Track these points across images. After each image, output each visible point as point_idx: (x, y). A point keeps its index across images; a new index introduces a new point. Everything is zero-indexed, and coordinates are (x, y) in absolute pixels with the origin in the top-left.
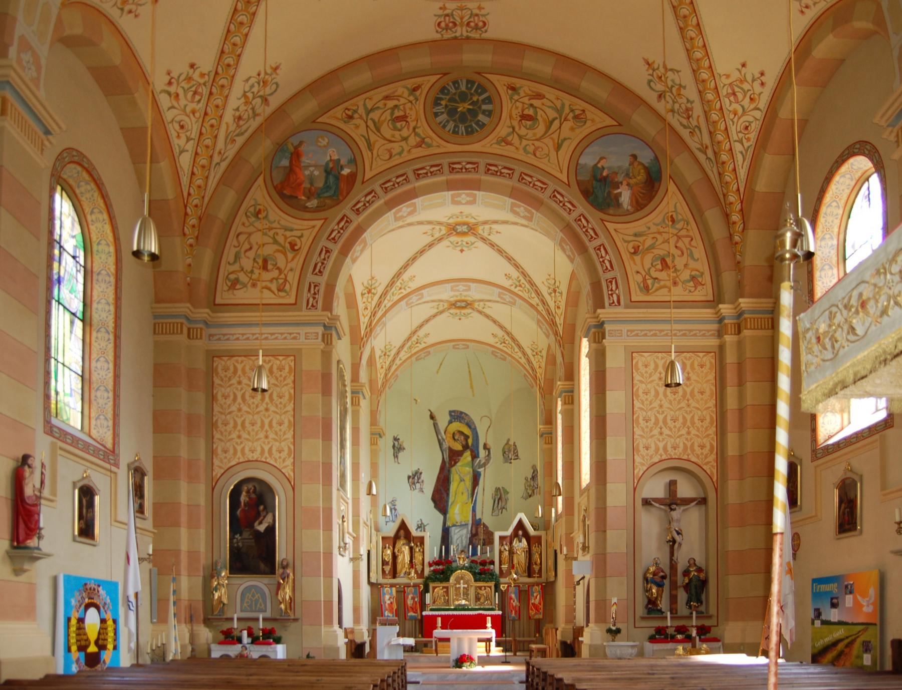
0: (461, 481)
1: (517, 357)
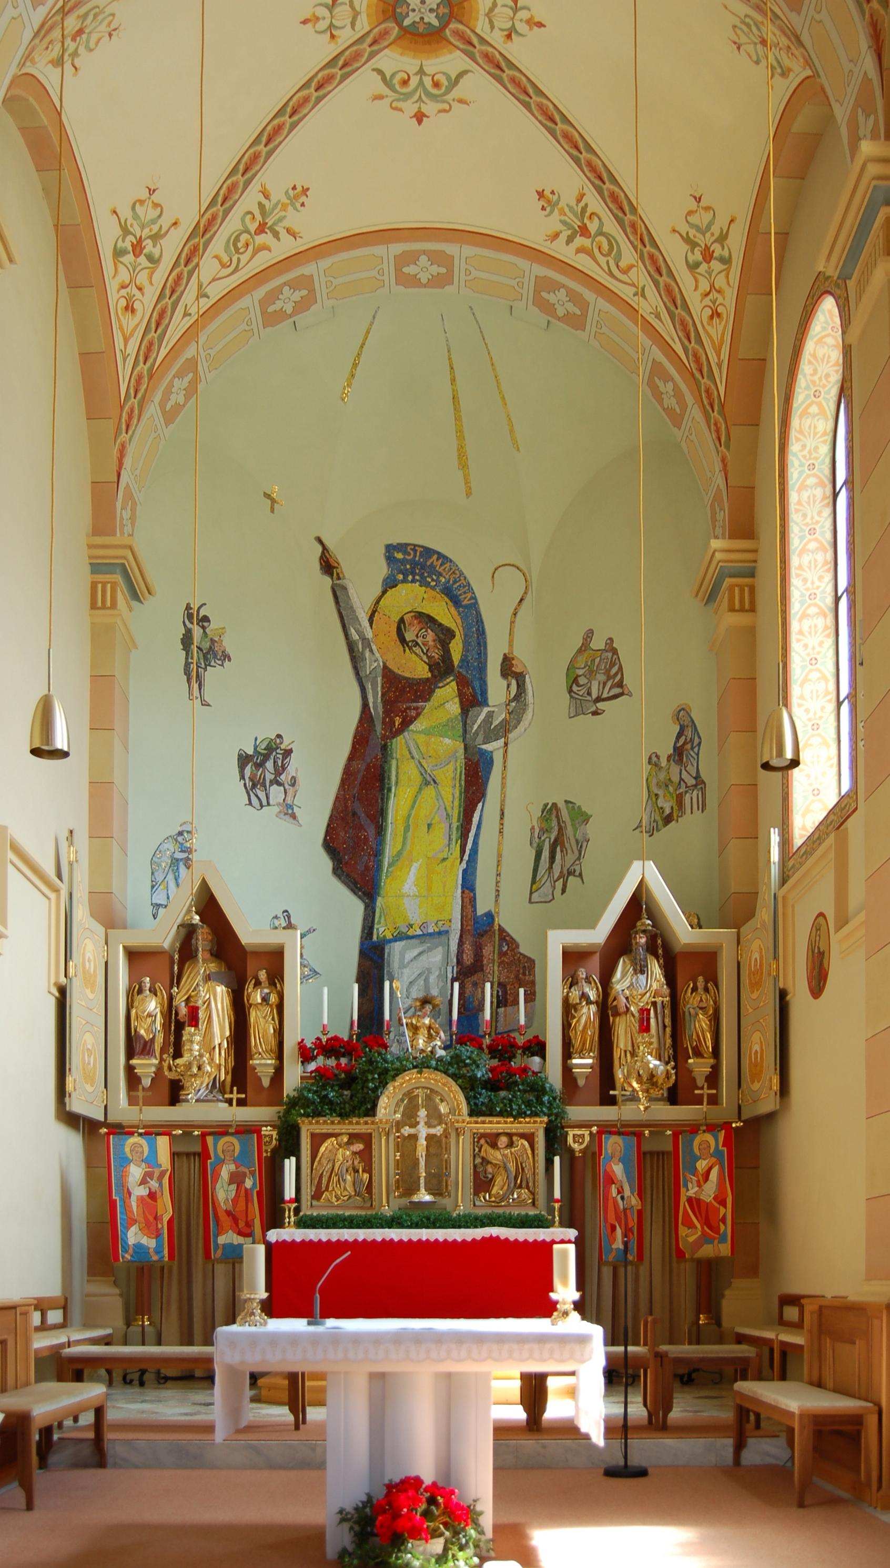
0: (427, 783)
1: (626, 292)
